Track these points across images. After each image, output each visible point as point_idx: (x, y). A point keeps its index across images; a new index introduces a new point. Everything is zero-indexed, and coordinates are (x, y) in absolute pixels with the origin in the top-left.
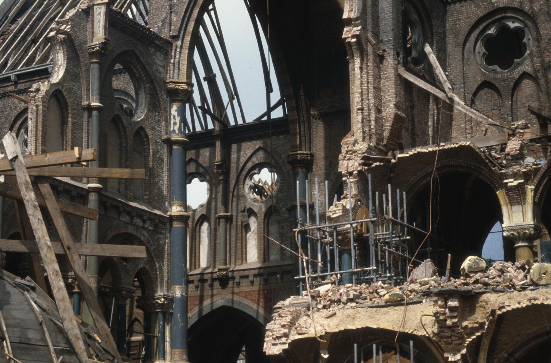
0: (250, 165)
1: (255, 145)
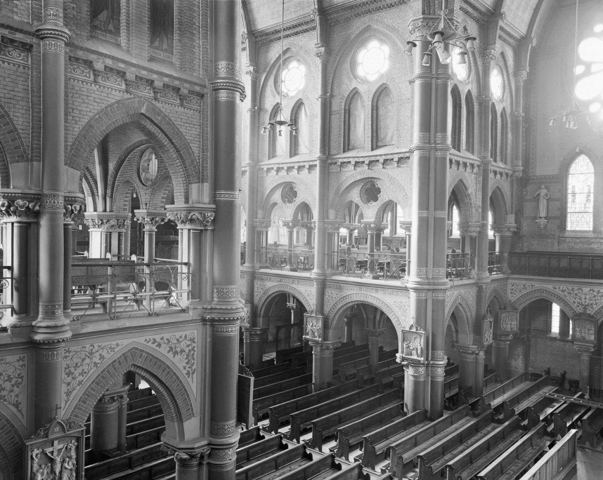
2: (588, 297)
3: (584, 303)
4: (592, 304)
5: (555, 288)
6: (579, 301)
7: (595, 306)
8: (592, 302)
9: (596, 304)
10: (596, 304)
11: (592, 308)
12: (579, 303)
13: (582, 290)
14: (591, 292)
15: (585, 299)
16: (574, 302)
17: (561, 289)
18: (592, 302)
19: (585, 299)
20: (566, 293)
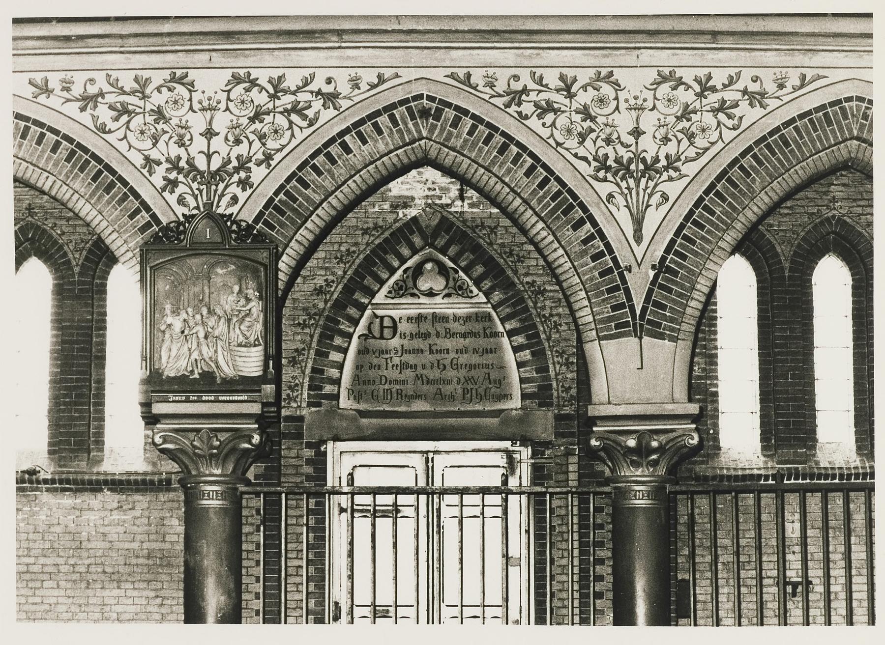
2: (222, 122)
3: (201, 163)
4: (243, 165)
5: (46, 90)
6: (175, 151)
7: (258, 173)
8: (242, 149)
9: (268, 157)
10: (268, 157)
11: (244, 184)
12: (175, 165)
13: (191, 87)
14: (239, 90)
15: (209, 134)
16: (150, 163)
17: (501, 87)
18: (242, 149)
19: (209, 134)
20: (104, 114)
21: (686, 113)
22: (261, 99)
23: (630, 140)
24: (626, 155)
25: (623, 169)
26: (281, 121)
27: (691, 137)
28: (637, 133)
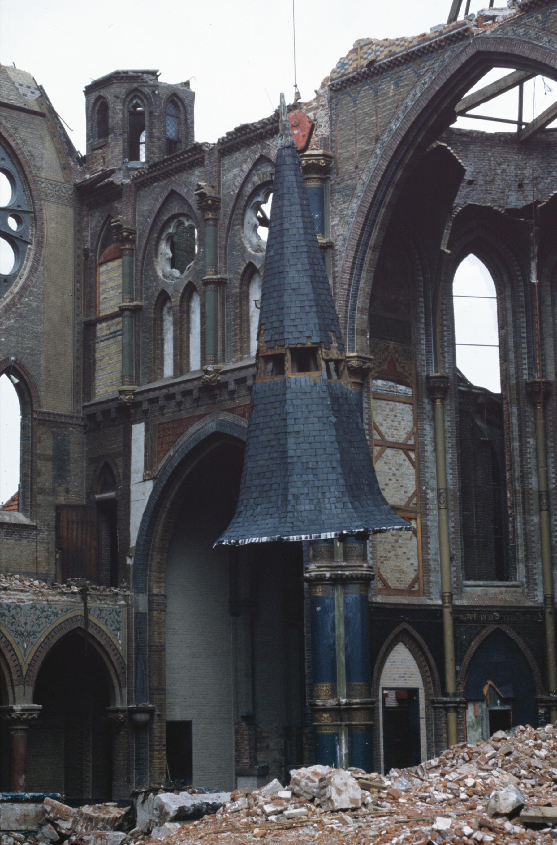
0: (249, 188)
1: (255, 153)
2: (29, 620)
21: (38, 618)
22: (38, 613)
23: (24, 626)
24: (23, 630)
25: (22, 635)
26: (43, 620)
27: (39, 625)
28: (26, 623)
